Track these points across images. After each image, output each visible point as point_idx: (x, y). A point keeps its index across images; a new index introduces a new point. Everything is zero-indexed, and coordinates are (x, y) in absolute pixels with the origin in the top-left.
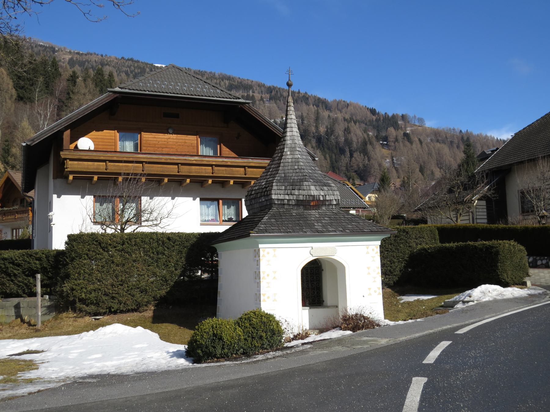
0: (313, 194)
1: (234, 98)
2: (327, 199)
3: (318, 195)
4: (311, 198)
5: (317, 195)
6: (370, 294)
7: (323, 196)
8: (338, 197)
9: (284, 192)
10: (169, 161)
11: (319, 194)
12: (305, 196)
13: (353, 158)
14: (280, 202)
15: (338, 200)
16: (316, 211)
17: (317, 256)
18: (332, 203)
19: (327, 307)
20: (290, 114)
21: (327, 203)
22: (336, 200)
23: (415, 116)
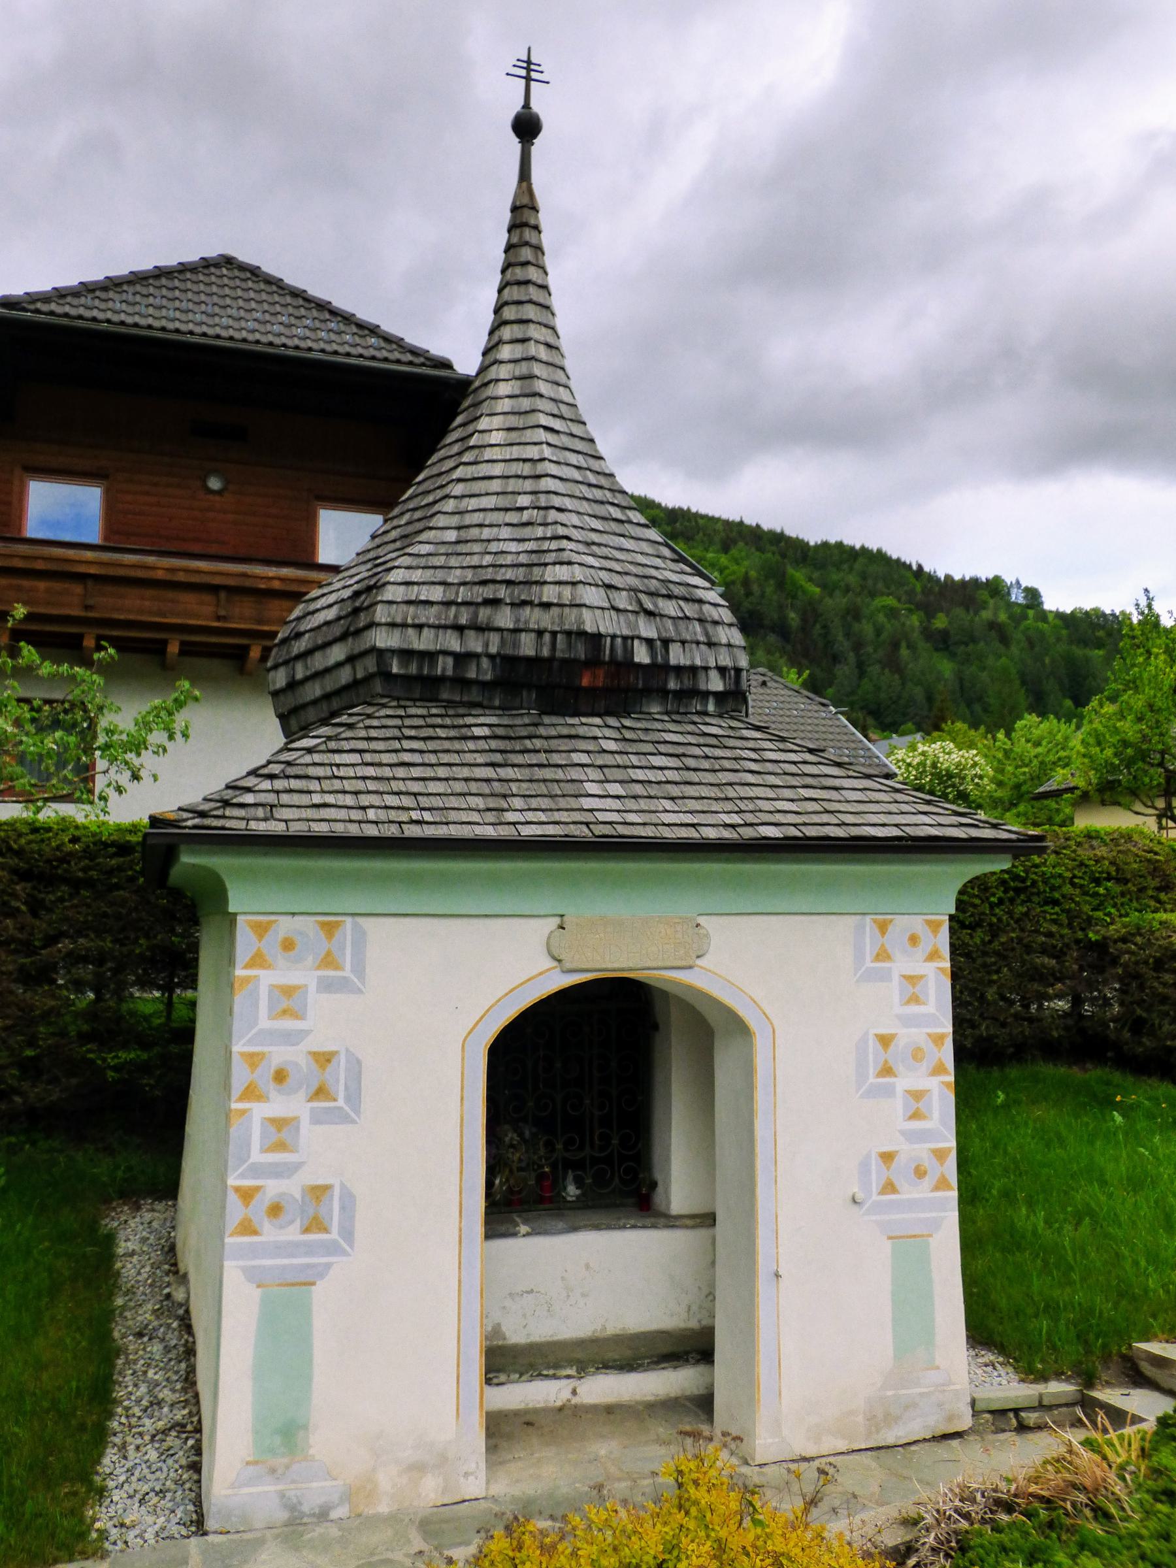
0: (589, 628)
1: (428, 363)
2: (673, 661)
3: (625, 638)
4: (581, 651)
5: (614, 637)
6: (889, 1187)
7: (649, 642)
8: (734, 659)
9: (438, 617)
10: (181, 577)
11: (626, 632)
12: (547, 637)
13: (866, 680)
14: (413, 669)
15: (738, 671)
16: (612, 721)
17: (598, 966)
18: (702, 687)
19: (671, 1222)
20: (522, 259)
21: (672, 685)
22: (722, 670)
23: (1018, 582)
